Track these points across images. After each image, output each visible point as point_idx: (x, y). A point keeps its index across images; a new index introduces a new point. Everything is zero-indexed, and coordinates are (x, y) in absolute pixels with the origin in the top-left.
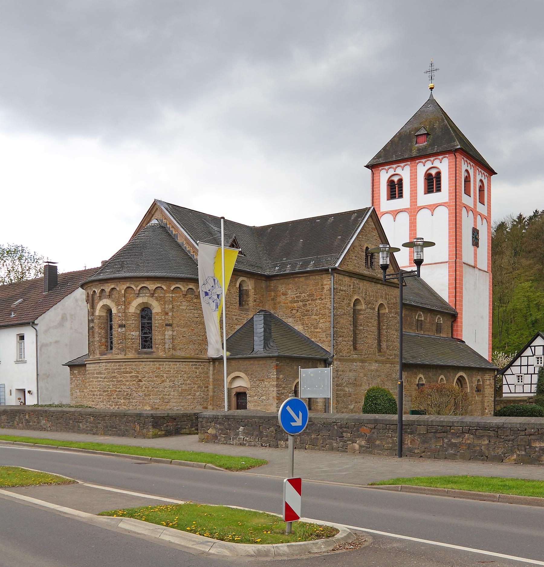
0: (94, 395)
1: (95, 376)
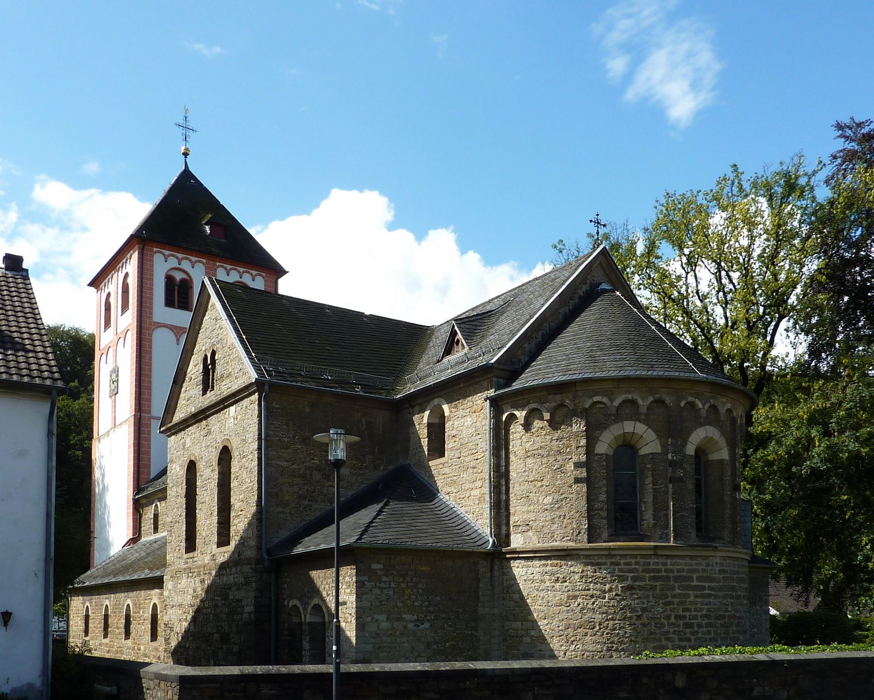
1: (693, 584)
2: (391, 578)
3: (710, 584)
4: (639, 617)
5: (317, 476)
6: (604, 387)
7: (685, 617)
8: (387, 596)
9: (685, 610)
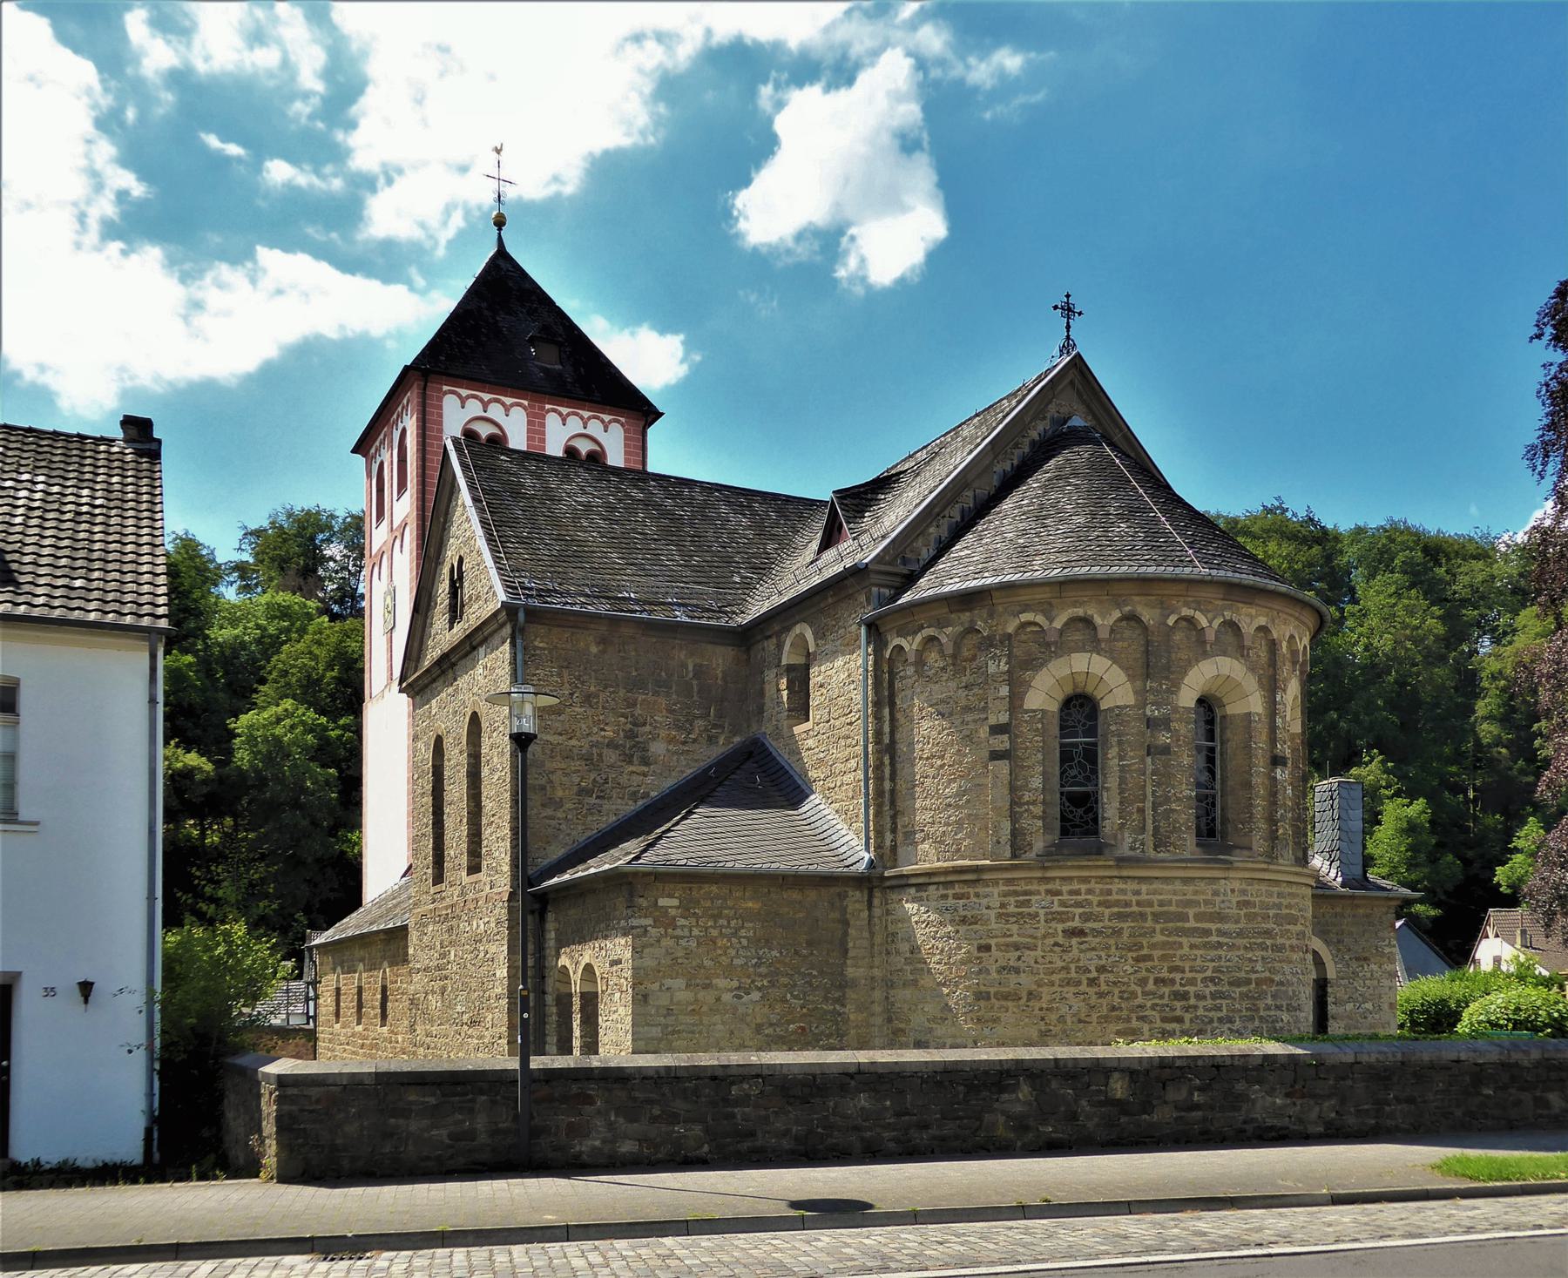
1: (1187, 925)
2: (693, 921)
3: (1219, 925)
4: (1092, 982)
5: (611, 756)
6: (1038, 596)
7: (1173, 981)
8: (686, 949)
9: (1172, 969)
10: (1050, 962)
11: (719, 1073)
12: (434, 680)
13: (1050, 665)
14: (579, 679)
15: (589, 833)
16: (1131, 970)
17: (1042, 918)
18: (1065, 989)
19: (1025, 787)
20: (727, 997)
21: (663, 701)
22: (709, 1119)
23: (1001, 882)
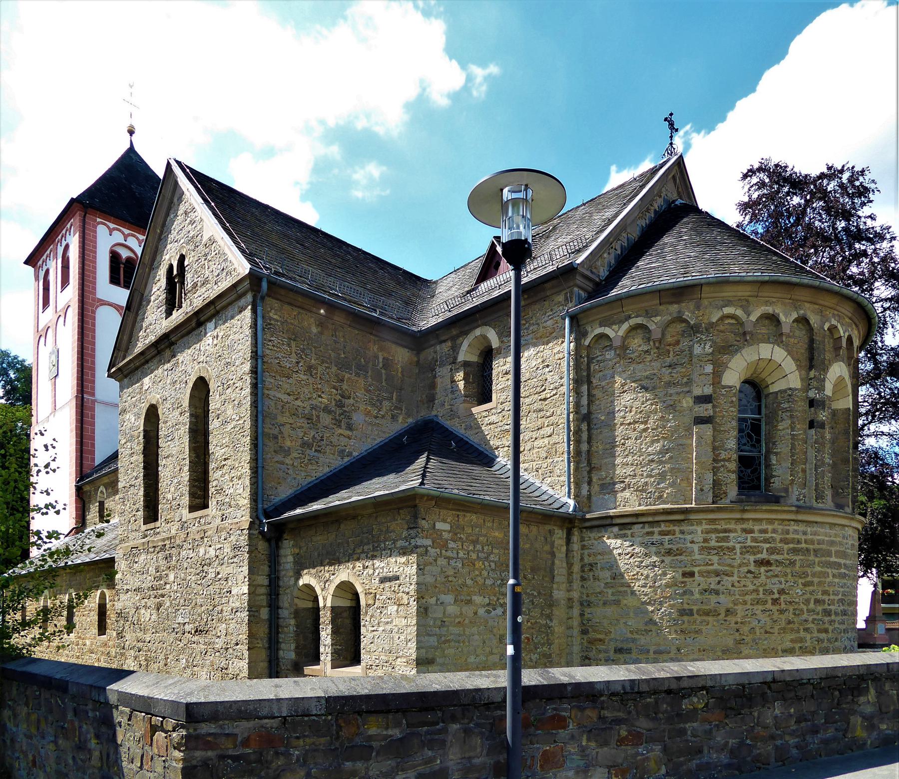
0: (828, 613)
4: (775, 601)
5: (326, 419)
6: (740, 294)
7: (824, 601)
9: (825, 593)
10: (744, 586)
11: (674, 686)
12: (147, 362)
13: (744, 352)
14: (303, 352)
15: (309, 479)
16: (801, 593)
17: (738, 551)
18: (755, 607)
19: (722, 447)
20: (481, 611)
21: (362, 382)
22: (666, 738)
23: (704, 522)
